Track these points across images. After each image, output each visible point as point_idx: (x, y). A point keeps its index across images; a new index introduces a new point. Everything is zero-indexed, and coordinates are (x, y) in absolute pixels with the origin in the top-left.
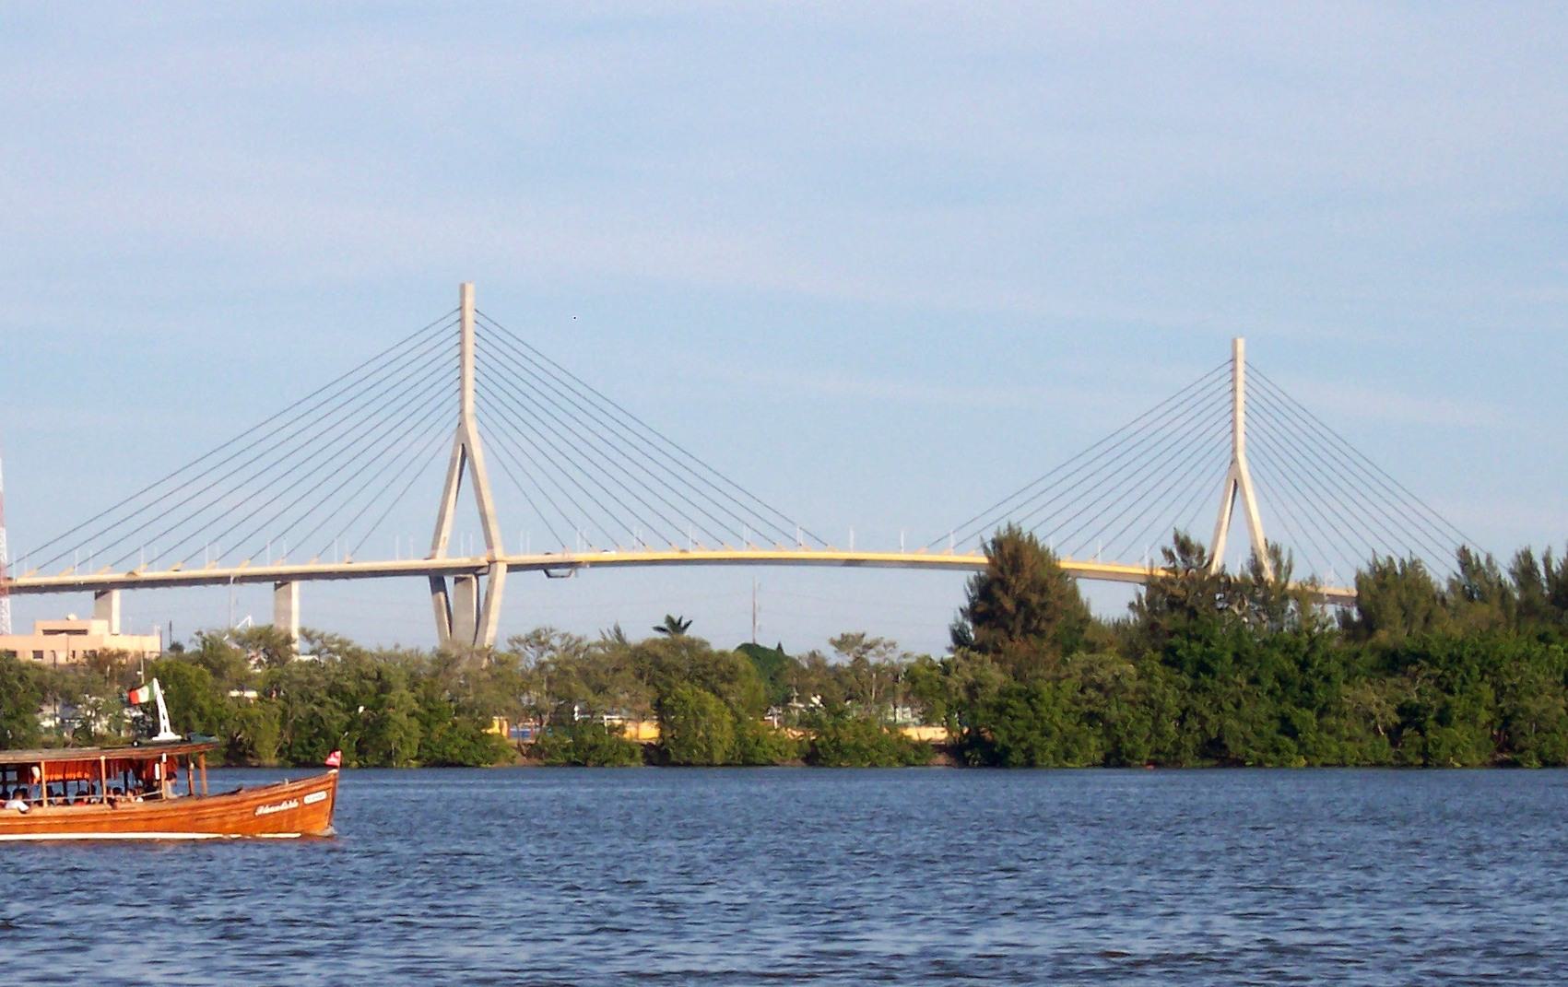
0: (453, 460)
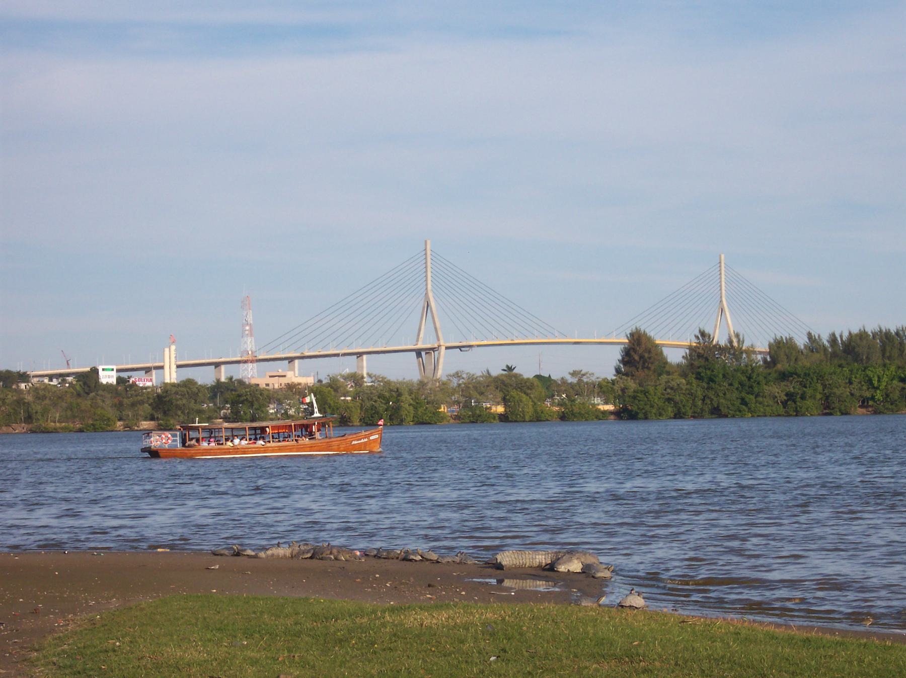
0: (424, 308)
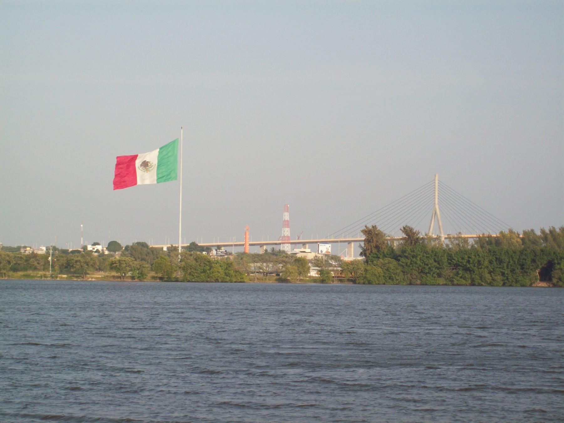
0: (433, 214)
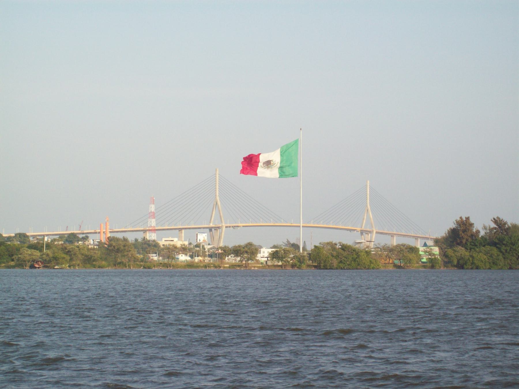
0: (214, 205)
